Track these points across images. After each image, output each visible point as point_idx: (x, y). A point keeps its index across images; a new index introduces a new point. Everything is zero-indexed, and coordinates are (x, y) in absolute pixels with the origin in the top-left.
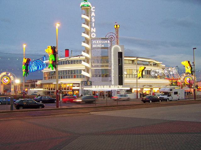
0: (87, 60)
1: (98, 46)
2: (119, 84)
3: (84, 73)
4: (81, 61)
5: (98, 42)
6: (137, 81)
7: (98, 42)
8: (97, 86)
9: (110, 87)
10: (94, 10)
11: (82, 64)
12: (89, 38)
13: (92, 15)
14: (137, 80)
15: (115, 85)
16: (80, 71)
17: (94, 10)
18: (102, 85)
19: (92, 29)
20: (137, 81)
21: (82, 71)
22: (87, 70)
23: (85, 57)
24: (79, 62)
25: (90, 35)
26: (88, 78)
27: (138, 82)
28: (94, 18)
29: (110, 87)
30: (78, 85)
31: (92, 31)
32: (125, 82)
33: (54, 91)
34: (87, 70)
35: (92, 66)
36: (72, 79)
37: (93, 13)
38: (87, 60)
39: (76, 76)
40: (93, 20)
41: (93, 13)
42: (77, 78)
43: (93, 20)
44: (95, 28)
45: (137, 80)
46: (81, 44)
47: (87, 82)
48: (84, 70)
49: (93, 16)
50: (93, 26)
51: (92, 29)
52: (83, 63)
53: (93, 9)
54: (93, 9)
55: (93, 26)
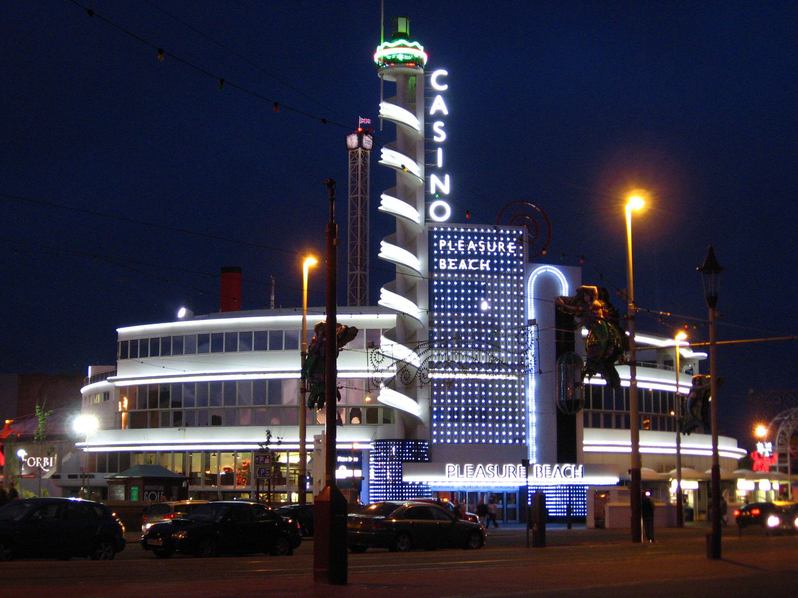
1: (463, 265)
2: (561, 460)
3: (390, 397)
4: (378, 388)
6: (679, 448)
7: (460, 244)
10: (445, 87)
12: (418, 221)
13: (432, 112)
17: (445, 87)
18: (494, 462)
19: (434, 179)
20: (679, 448)
21: (382, 385)
22: (406, 380)
23: (394, 317)
26: (408, 420)
27: (682, 452)
28: (442, 124)
30: (356, 459)
31: (433, 191)
32: (585, 449)
38: (404, 332)
40: (440, 136)
42: (127, 342)
43: (438, 136)
44: (447, 177)
46: (378, 202)
47: (411, 444)
48: (390, 384)
49: (439, 116)
50: (440, 163)
51: (434, 179)
52: (386, 344)
53: (441, 80)
54: (441, 80)
55: (440, 163)
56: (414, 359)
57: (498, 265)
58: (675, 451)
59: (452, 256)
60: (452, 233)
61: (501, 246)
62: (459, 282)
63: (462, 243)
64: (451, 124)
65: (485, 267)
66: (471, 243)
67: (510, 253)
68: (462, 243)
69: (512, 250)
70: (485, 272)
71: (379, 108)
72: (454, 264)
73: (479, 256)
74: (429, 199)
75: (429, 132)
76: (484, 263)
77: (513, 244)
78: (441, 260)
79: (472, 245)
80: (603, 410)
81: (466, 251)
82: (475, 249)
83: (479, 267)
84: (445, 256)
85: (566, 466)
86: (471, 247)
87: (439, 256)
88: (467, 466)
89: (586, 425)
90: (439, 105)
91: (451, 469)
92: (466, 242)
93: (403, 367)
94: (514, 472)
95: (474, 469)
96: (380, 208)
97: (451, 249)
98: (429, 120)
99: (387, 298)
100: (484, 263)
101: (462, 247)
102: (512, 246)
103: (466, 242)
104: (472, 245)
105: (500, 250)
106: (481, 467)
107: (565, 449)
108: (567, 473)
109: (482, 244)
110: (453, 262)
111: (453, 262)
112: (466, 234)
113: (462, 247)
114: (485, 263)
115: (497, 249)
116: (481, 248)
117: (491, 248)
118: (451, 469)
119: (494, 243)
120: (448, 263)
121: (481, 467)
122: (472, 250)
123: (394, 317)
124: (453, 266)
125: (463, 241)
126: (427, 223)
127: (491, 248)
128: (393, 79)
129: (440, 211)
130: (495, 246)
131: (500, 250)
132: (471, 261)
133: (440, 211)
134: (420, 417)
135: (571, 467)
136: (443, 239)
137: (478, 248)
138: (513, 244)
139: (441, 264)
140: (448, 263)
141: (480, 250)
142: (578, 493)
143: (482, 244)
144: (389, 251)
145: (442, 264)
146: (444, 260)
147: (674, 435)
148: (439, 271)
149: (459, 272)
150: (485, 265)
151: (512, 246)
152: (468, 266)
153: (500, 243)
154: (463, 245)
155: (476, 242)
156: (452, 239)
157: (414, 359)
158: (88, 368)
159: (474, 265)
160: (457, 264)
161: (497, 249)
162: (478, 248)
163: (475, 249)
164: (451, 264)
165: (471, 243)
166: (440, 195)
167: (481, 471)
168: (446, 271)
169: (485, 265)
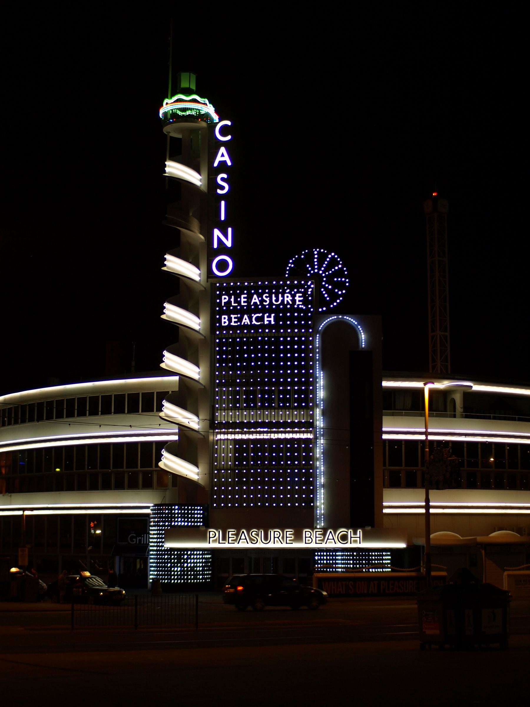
0: (185, 395)
1: (246, 320)
3: (170, 462)
5: (243, 299)
6: (427, 507)
7: (243, 299)
8: (231, 532)
9: (298, 537)
11: (162, 414)
12: (197, 279)
14: (427, 501)
15: (334, 523)
16: (151, 451)
20: (427, 507)
22: (187, 446)
24: (147, 403)
25: (204, 268)
29: (298, 537)
33: (233, 322)
34: (187, 446)
35: (213, 425)
36: (17, 426)
37: (223, 150)
38: (185, 395)
39: (402, 475)
41: (223, 150)
45: (427, 501)
54: (224, 131)
56: (193, 421)
57: (285, 318)
58: (423, 511)
59: (235, 311)
60: (235, 288)
61: (288, 298)
62: (292, 338)
63: (244, 298)
64: (233, 173)
65: (270, 321)
66: (255, 296)
67: (233, 306)
68: (244, 298)
69: (299, 301)
70: (269, 325)
71: (165, 166)
72: (236, 320)
73: (264, 310)
74: (213, 253)
75: (213, 184)
76: (268, 317)
77: (301, 295)
78: (223, 317)
79: (255, 299)
80: (125, 469)
81: (249, 305)
82: (258, 303)
83: (264, 321)
84: (228, 313)
85: (342, 531)
86: (255, 301)
87: (222, 312)
88: (316, 532)
89: (385, 486)
90: (223, 156)
91: (308, 534)
92: (250, 298)
93: (184, 430)
94: (280, 538)
95: (237, 535)
96: (164, 268)
97: (233, 304)
98: (213, 173)
99: (171, 361)
100: (268, 317)
101: (244, 302)
102: (299, 297)
103: (250, 298)
104: (255, 299)
105: (286, 303)
106: (331, 532)
107: (358, 510)
108: (344, 538)
109: (266, 297)
110: (235, 318)
111: (235, 318)
112: (249, 288)
113: (244, 302)
114: (269, 317)
115: (283, 301)
116: (266, 301)
117: (277, 300)
118: (308, 534)
119: (280, 295)
120: (230, 320)
121: (243, 532)
122: (255, 303)
123: (177, 378)
124: (235, 322)
125: (246, 296)
126: (209, 279)
127: (277, 300)
128: (180, 136)
129: (222, 266)
130: (281, 298)
131: (286, 303)
132: (254, 316)
133: (222, 266)
134: (200, 482)
135: (347, 532)
136: (288, 293)
137: (262, 301)
138: (301, 295)
139: (223, 320)
140: (230, 320)
141: (264, 303)
142: (197, 559)
143: (266, 297)
144: (173, 312)
145: (225, 320)
146: (226, 317)
147: (423, 492)
148: (221, 328)
149: (242, 327)
150: (269, 319)
151: (299, 297)
152: (251, 321)
153: (286, 295)
154: (246, 300)
155: (260, 295)
156: (235, 294)
157: (193, 421)
158: (385, 440)
159: (257, 319)
160: (240, 319)
161: (283, 301)
162: (262, 301)
163: (258, 303)
164: (233, 320)
165: (255, 296)
166: (222, 249)
167: (331, 537)
168: (229, 327)
169: (269, 319)
